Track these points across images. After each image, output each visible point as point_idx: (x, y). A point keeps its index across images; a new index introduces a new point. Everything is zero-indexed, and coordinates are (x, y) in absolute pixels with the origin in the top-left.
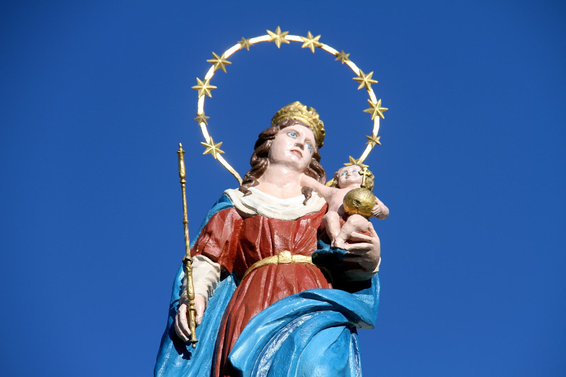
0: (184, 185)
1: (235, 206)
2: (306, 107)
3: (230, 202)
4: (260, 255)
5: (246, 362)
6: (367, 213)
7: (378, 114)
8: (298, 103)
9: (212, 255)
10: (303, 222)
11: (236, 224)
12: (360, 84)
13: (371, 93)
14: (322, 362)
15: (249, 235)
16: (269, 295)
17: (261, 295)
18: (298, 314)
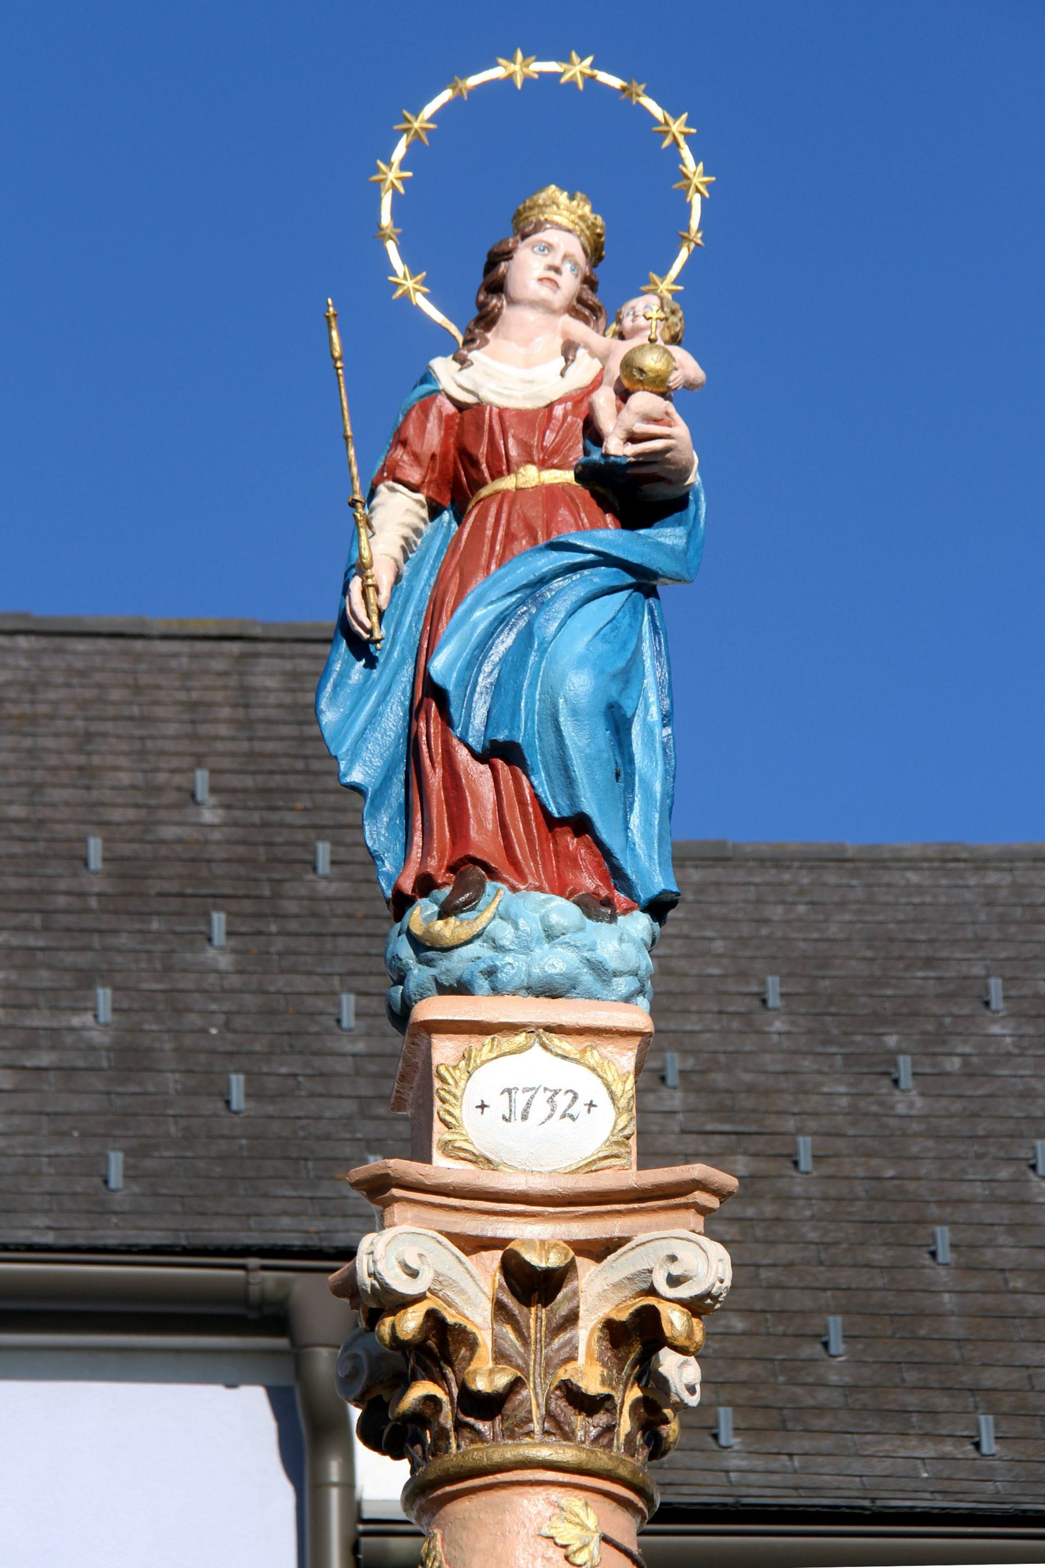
0: (340, 371)
1: (443, 390)
2: (565, 194)
3: (436, 384)
4: (487, 475)
5: (455, 675)
6: (658, 387)
7: (698, 190)
8: (553, 187)
9: (409, 482)
10: (558, 411)
11: (447, 422)
12: (664, 139)
13: (686, 152)
14: (581, 663)
15: (469, 441)
16: (498, 548)
17: (486, 549)
18: (543, 581)
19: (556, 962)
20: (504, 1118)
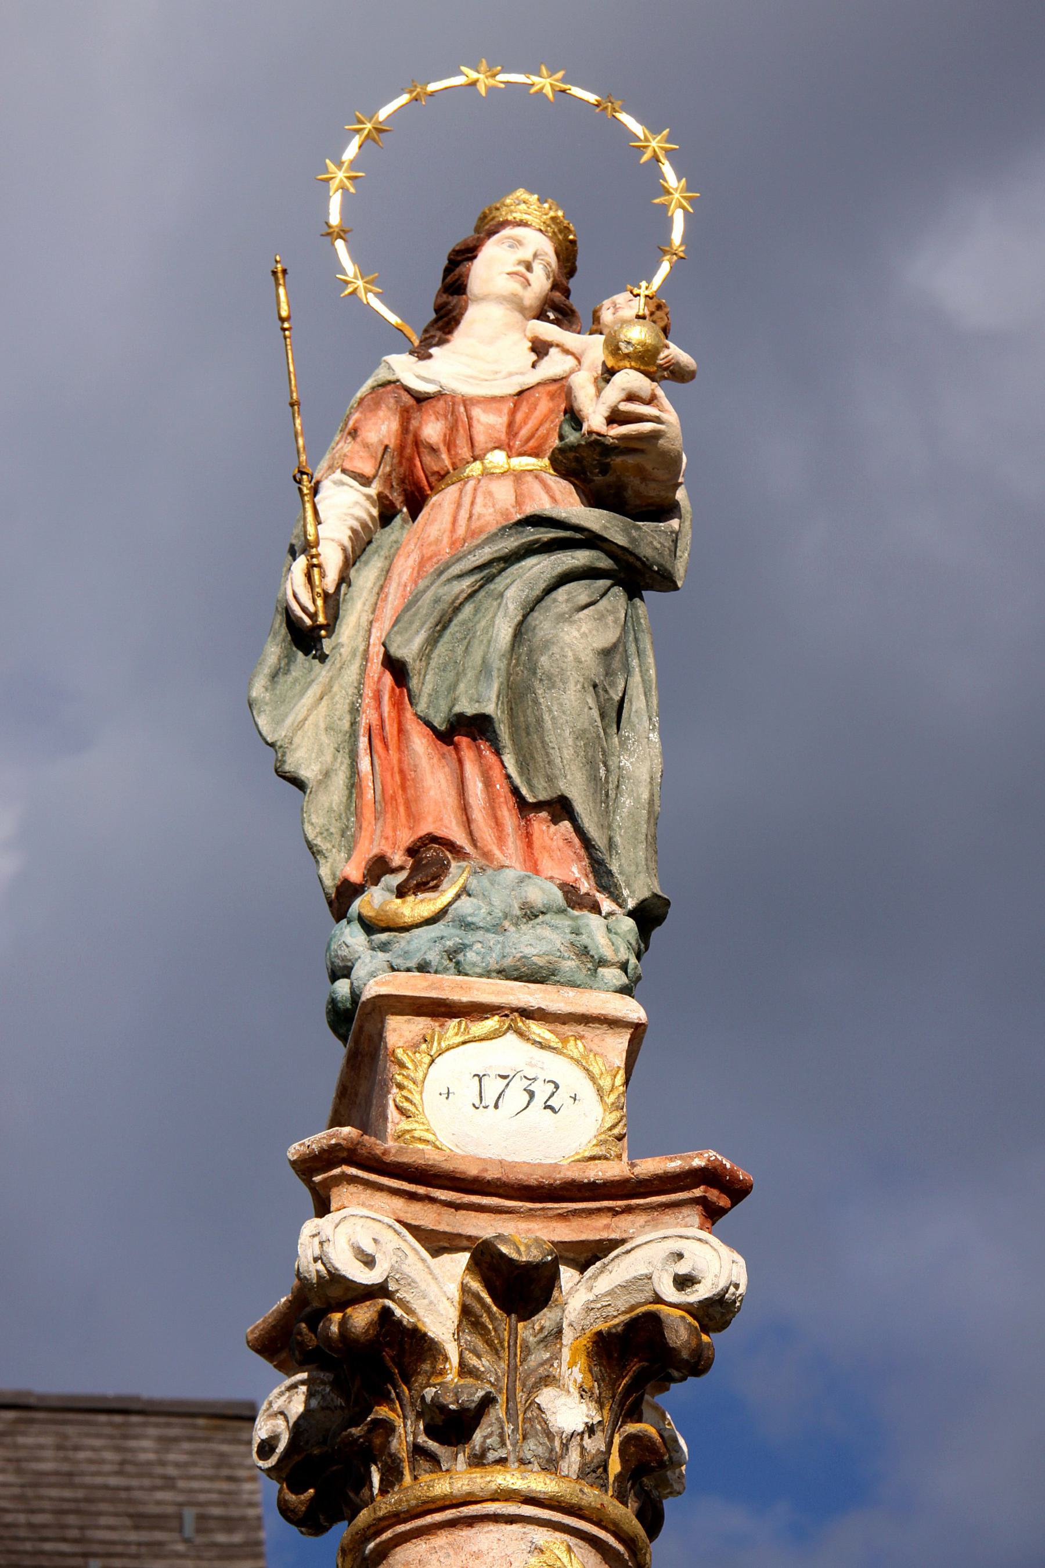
2: (536, 196)
6: (647, 364)
12: (644, 153)
19: (537, 942)
20: (474, 1105)
